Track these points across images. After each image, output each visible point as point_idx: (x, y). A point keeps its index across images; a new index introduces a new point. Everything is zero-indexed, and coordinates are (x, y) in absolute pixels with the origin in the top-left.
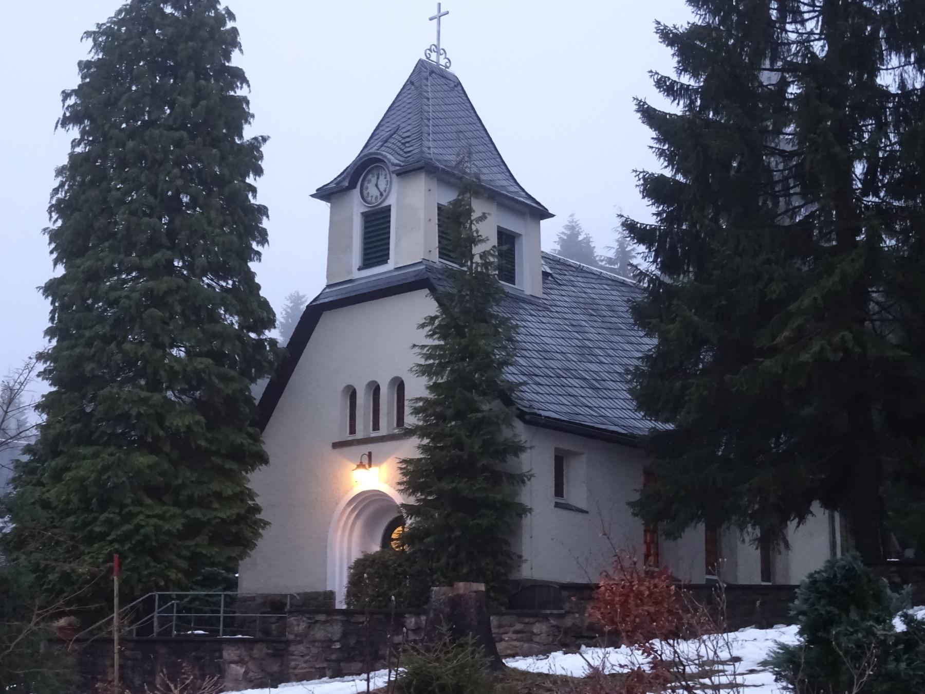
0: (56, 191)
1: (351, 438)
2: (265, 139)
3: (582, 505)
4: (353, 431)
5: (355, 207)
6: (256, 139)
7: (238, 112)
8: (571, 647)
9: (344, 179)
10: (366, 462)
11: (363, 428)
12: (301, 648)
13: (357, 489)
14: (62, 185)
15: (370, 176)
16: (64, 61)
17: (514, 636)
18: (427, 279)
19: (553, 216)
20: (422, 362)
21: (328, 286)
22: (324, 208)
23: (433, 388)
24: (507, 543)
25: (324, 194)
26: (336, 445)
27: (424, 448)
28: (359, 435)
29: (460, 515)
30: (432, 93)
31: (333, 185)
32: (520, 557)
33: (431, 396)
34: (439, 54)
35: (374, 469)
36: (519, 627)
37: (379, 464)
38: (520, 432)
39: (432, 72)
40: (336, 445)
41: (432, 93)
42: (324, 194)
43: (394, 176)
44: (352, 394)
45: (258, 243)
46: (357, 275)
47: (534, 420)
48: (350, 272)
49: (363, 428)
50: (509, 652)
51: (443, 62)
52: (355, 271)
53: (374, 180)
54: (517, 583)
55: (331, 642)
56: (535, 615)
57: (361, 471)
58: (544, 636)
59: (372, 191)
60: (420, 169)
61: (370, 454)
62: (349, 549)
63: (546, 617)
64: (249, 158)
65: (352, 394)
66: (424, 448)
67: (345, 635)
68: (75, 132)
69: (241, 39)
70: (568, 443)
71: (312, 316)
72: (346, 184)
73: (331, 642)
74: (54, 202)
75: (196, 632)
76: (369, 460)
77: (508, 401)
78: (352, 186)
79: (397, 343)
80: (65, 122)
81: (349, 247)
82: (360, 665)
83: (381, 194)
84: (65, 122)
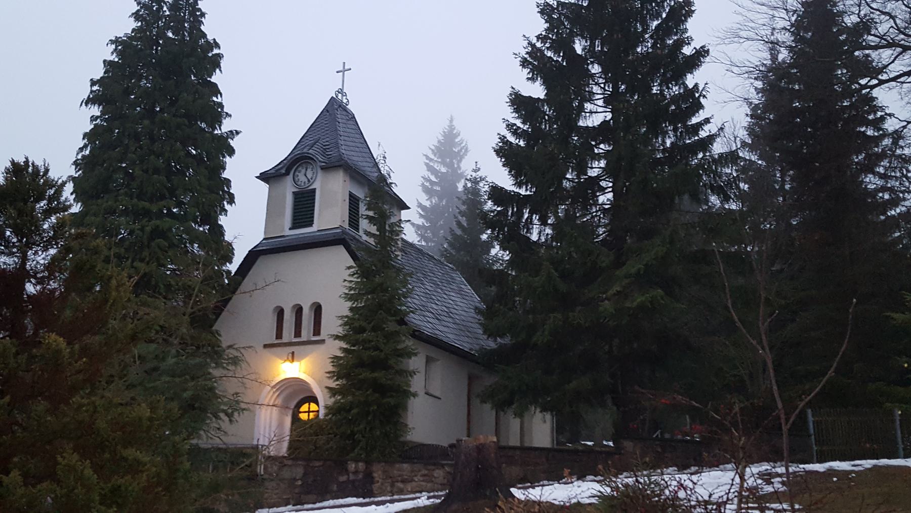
0: (81, 149)
1: (279, 341)
2: (238, 133)
3: (437, 394)
4: (279, 335)
5: (288, 189)
6: (231, 131)
7: (216, 114)
8: (821, 461)
9: (282, 168)
10: (290, 358)
11: (288, 334)
12: (274, 484)
13: (282, 377)
14: (85, 146)
15: (300, 169)
16: (94, 59)
17: (421, 479)
18: (344, 239)
19: (409, 208)
20: (347, 291)
21: (264, 239)
22: (264, 187)
23: (351, 309)
24: (400, 416)
25: (265, 177)
26: (266, 346)
27: (345, 350)
28: (285, 339)
29: (377, 395)
30: (335, 117)
31: (272, 171)
32: (406, 425)
33: (350, 314)
34: (343, 96)
35: (296, 364)
36: (424, 472)
37: (299, 360)
38: (410, 343)
39: (340, 106)
40: (266, 346)
41: (335, 117)
42: (265, 177)
43: (319, 169)
44: (280, 313)
45: (228, 203)
46: (288, 232)
47: (418, 335)
48: (283, 230)
49: (288, 334)
50: (418, 489)
51: (345, 101)
52: (285, 228)
53: (303, 171)
54: (405, 443)
55: (295, 480)
56: (434, 464)
57: (288, 364)
58: (441, 478)
59: (302, 178)
60: (340, 166)
61: (293, 353)
62: (271, 418)
63: (443, 466)
64: (223, 147)
65: (280, 313)
66: (345, 350)
67: (305, 474)
68: (96, 111)
69: (223, 63)
70: (434, 352)
71: (253, 256)
72: (283, 171)
73: (295, 480)
74: (79, 157)
75: (812, 431)
76: (293, 357)
77: (402, 322)
78: (287, 173)
79: (326, 282)
80: (89, 101)
81: (282, 214)
82: (315, 497)
83: (309, 181)
84: (89, 101)
